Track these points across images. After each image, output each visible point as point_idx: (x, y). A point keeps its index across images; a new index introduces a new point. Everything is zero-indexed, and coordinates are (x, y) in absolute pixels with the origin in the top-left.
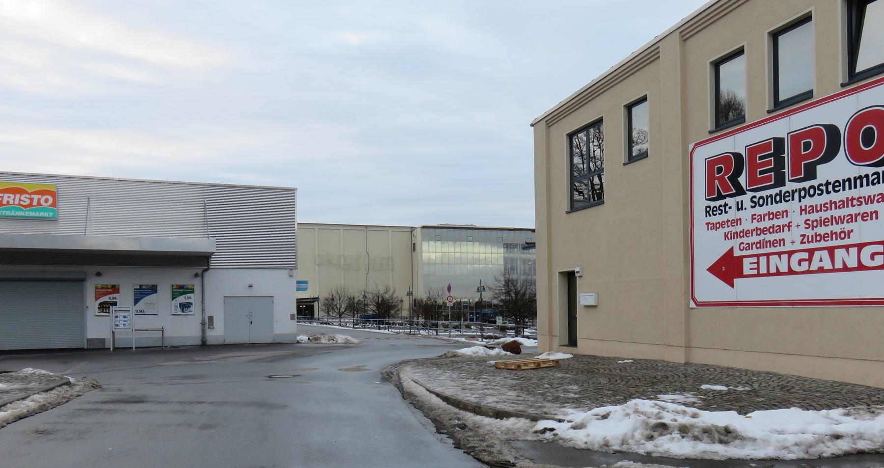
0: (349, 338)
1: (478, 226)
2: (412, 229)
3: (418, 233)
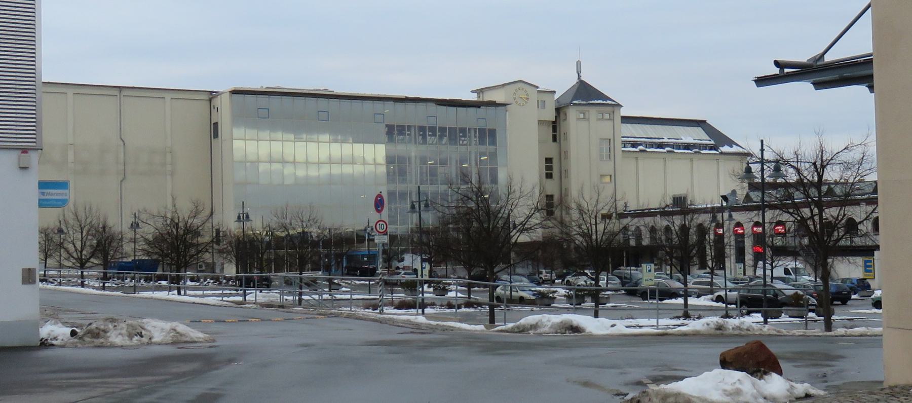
0: (182, 328)
1: (338, 90)
2: (212, 96)
3: (224, 104)
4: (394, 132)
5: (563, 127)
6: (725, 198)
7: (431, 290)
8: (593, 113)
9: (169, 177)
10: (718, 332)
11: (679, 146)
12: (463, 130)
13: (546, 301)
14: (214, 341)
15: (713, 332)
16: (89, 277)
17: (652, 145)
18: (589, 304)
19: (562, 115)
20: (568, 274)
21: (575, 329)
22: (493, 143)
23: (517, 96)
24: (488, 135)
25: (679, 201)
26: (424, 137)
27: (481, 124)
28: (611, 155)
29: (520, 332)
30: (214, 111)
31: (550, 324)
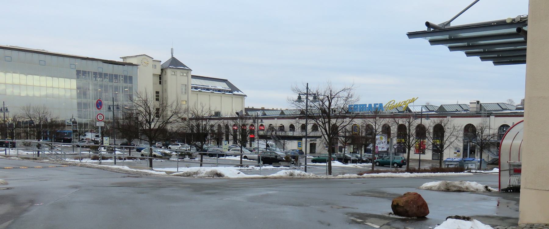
4: (80, 74)
5: (164, 77)
6: (237, 113)
7: (105, 150)
8: (178, 72)
10: (291, 177)
11: (216, 90)
12: (116, 76)
13: (167, 157)
14: (7, 184)
15: (288, 176)
17: (204, 89)
18: (187, 158)
19: (164, 72)
20: (169, 144)
21: (219, 175)
22: (131, 83)
24: (129, 79)
25: (217, 114)
26: (96, 77)
27: (125, 73)
28: (186, 92)
29: (187, 176)
31: (205, 172)
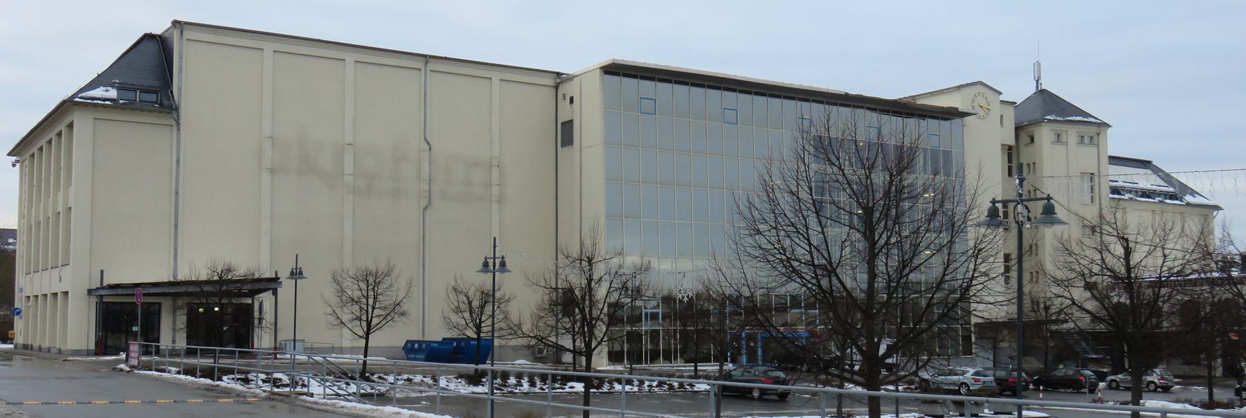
2: (560, 79)
8: (1072, 134)
9: (495, 206)
16: (352, 350)
23: (976, 104)
30: (564, 105)
